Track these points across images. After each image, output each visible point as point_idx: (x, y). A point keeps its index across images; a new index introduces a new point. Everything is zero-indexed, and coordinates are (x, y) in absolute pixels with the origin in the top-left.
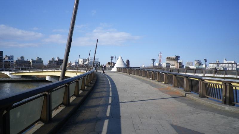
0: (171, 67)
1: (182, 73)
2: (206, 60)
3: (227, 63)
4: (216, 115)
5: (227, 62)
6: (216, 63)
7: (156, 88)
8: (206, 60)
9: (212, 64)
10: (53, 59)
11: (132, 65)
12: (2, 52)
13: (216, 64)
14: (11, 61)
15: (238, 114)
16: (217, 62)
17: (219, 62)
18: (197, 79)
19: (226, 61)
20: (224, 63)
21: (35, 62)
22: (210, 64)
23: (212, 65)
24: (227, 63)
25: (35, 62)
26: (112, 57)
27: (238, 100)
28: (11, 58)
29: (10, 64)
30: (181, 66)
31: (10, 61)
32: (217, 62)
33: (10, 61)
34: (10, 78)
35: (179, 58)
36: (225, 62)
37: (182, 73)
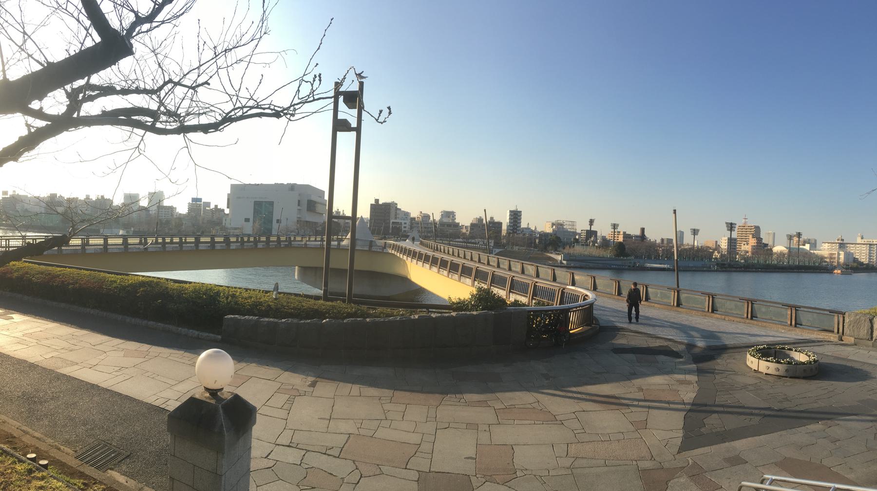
0: (547, 243)
1: (682, 367)
3: (864, 244)
6: (836, 241)
7: (61, 374)
9: (828, 243)
12: (192, 198)
14: (403, 223)
15: (249, 490)
16: (838, 240)
17: (843, 240)
18: (648, 265)
19: (862, 238)
22: (823, 244)
23: (828, 246)
24: (864, 244)
26: (591, 220)
29: (403, 227)
30: (760, 246)
31: (401, 223)
32: (838, 240)
33: (401, 223)
36: (859, 240)
37: (682, 367)
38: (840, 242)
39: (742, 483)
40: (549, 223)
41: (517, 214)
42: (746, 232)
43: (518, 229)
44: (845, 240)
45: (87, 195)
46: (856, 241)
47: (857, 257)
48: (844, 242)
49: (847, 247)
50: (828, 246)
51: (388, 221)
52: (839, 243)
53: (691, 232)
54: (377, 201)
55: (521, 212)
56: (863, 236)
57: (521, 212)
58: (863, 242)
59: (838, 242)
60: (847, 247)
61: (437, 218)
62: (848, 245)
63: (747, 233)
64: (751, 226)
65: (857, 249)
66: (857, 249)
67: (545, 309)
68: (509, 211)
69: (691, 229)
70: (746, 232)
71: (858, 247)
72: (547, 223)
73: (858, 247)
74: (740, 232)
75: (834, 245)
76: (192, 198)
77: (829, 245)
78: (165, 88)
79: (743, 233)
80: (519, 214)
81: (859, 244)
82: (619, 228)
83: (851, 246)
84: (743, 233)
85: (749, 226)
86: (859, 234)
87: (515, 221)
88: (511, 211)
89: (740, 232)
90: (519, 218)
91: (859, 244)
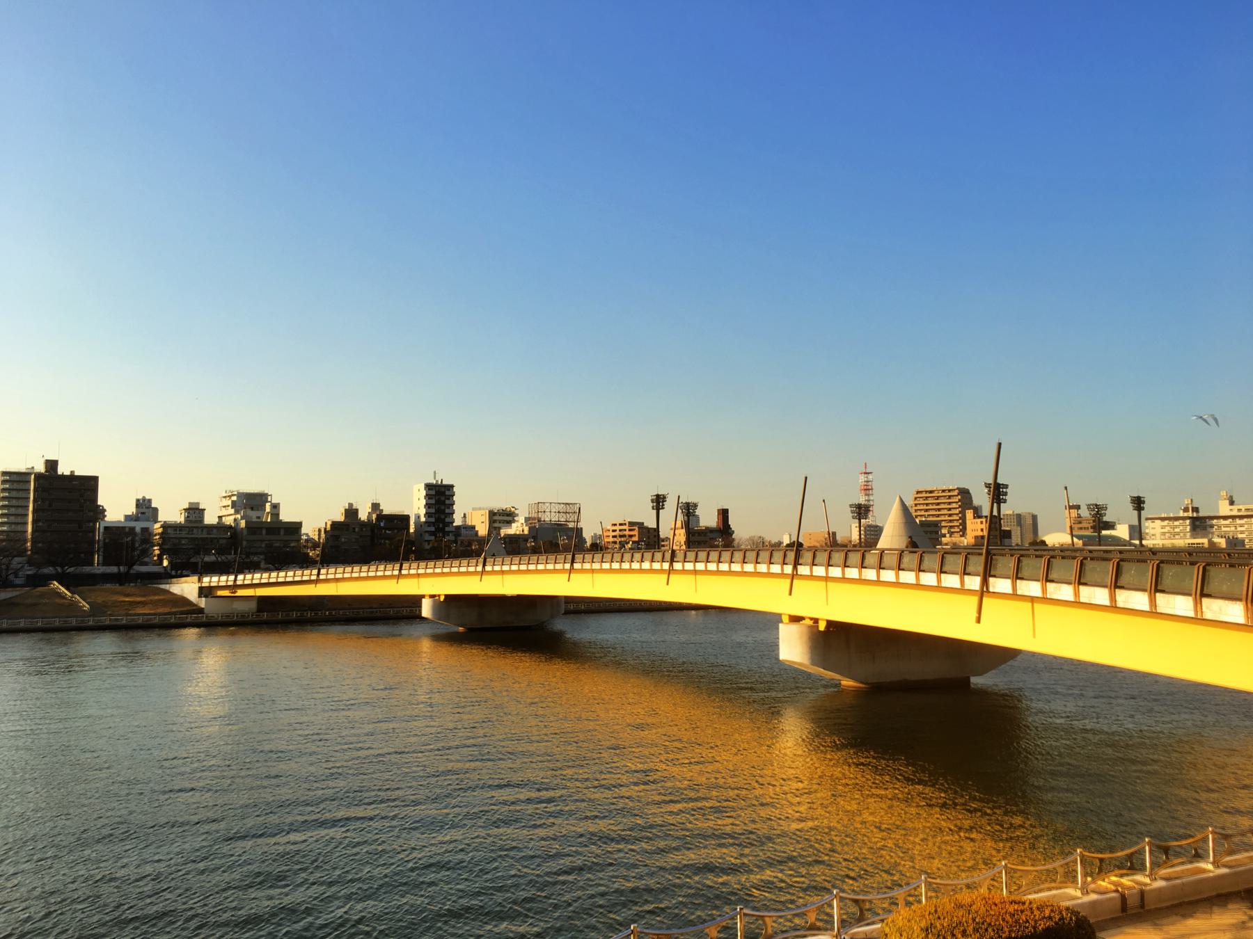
2: (1138, 503)
4: (1000, 668)
5: (1235, 507)
6: (1181, 514)
8: (1138, 503)
9: (1163, 519)
10: (351, 512)
11: (839, 538)
12: (95, 479)
13: (1184, 518)
16: (1186, 510)
17: (1196, 510)
19: (1232, 503)
20: (1222, 514)
21: (282, 532)
23: (1163, 527)
24: (1241, 517)
25: (282, 532)
26: (658, 496)
27: (478, 507)
28: (145, 508)
32: (1186, 510)
34: (201, 611)
35: (1006, 494)
38: (1190, 514)
39: (135, 567)
40: (483, 512)
41: (443, 494)
42: (938, 504)
43: (447, 529)
44: (1200, 510)
45: (349, 504)
46: (1218, 512)
47: (1240, 536)
48: (1201, 514)
49: (1212, 526)
50: (1163, 527)
51: (91, 534)
52: (1190, 518)
53: (852, 512)
54: (52, 465)
55: (452, 486)
56: (1231, 497)
57: (452, 486)
58: (1235, 513)
59: (1186, 514)
60: (1212, 526)
61: (181, 519)
62: (1215, 522)
63: (942, 512)
64: (949, 491)
65: (1239, 529)
66: (1239, 529)
67: (456, 566)
68: (422, 487)
69: (851, 506)
70: (938, 504)
71: (1241, 526)
72: (474, 512)
73: (1241, 526)
74: (922, 507)
75: (1177, 523)
76: (95, 479)
77: (1166, 523)
78: (224, 584)
79: (930, 507)
80: (447, 493)
81: (1225, 518)
82: (870, 515)
83: (1223, 522)
84: (930, 507)
85: (943, 491)
86: (1223, 493)
87: (439, 511)
88: (429, 487)
89: (922, 507)
90: (447, 502)
91: (1225, 518)
